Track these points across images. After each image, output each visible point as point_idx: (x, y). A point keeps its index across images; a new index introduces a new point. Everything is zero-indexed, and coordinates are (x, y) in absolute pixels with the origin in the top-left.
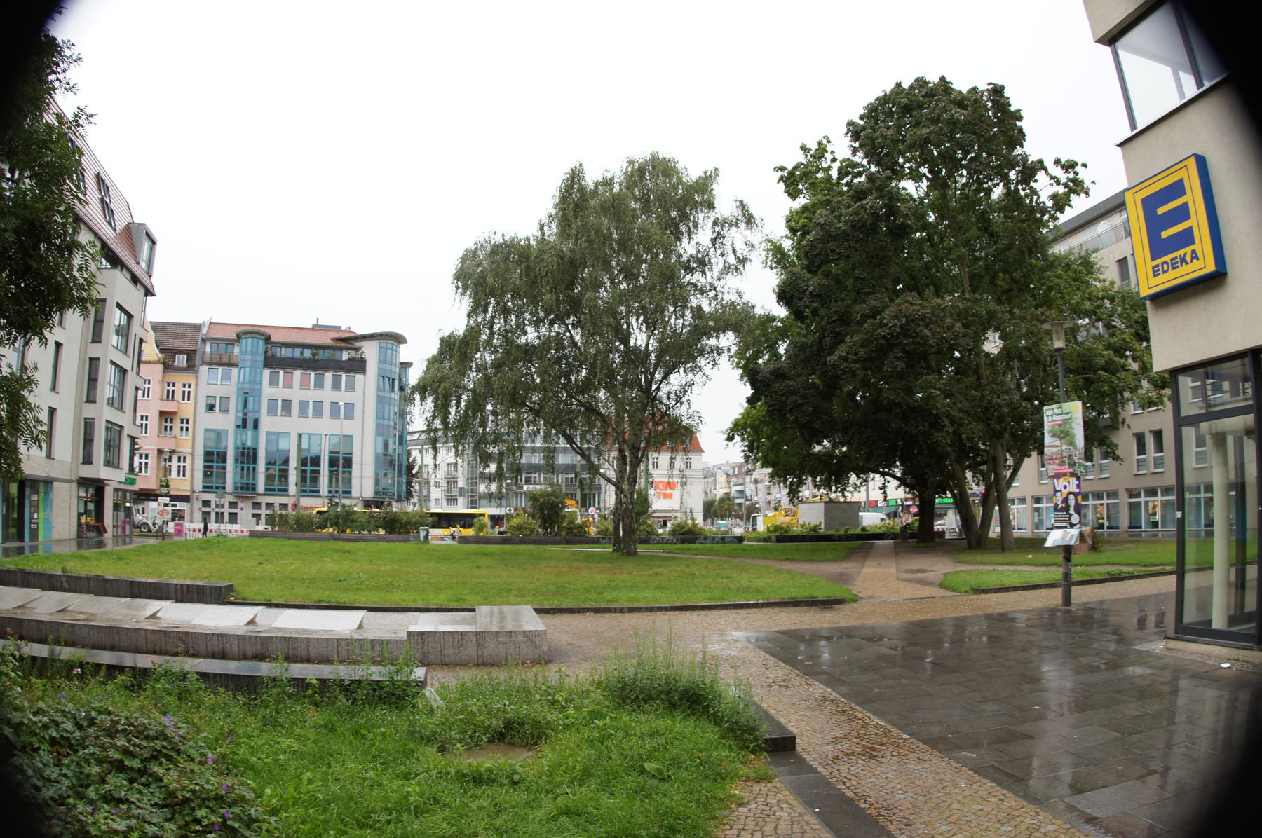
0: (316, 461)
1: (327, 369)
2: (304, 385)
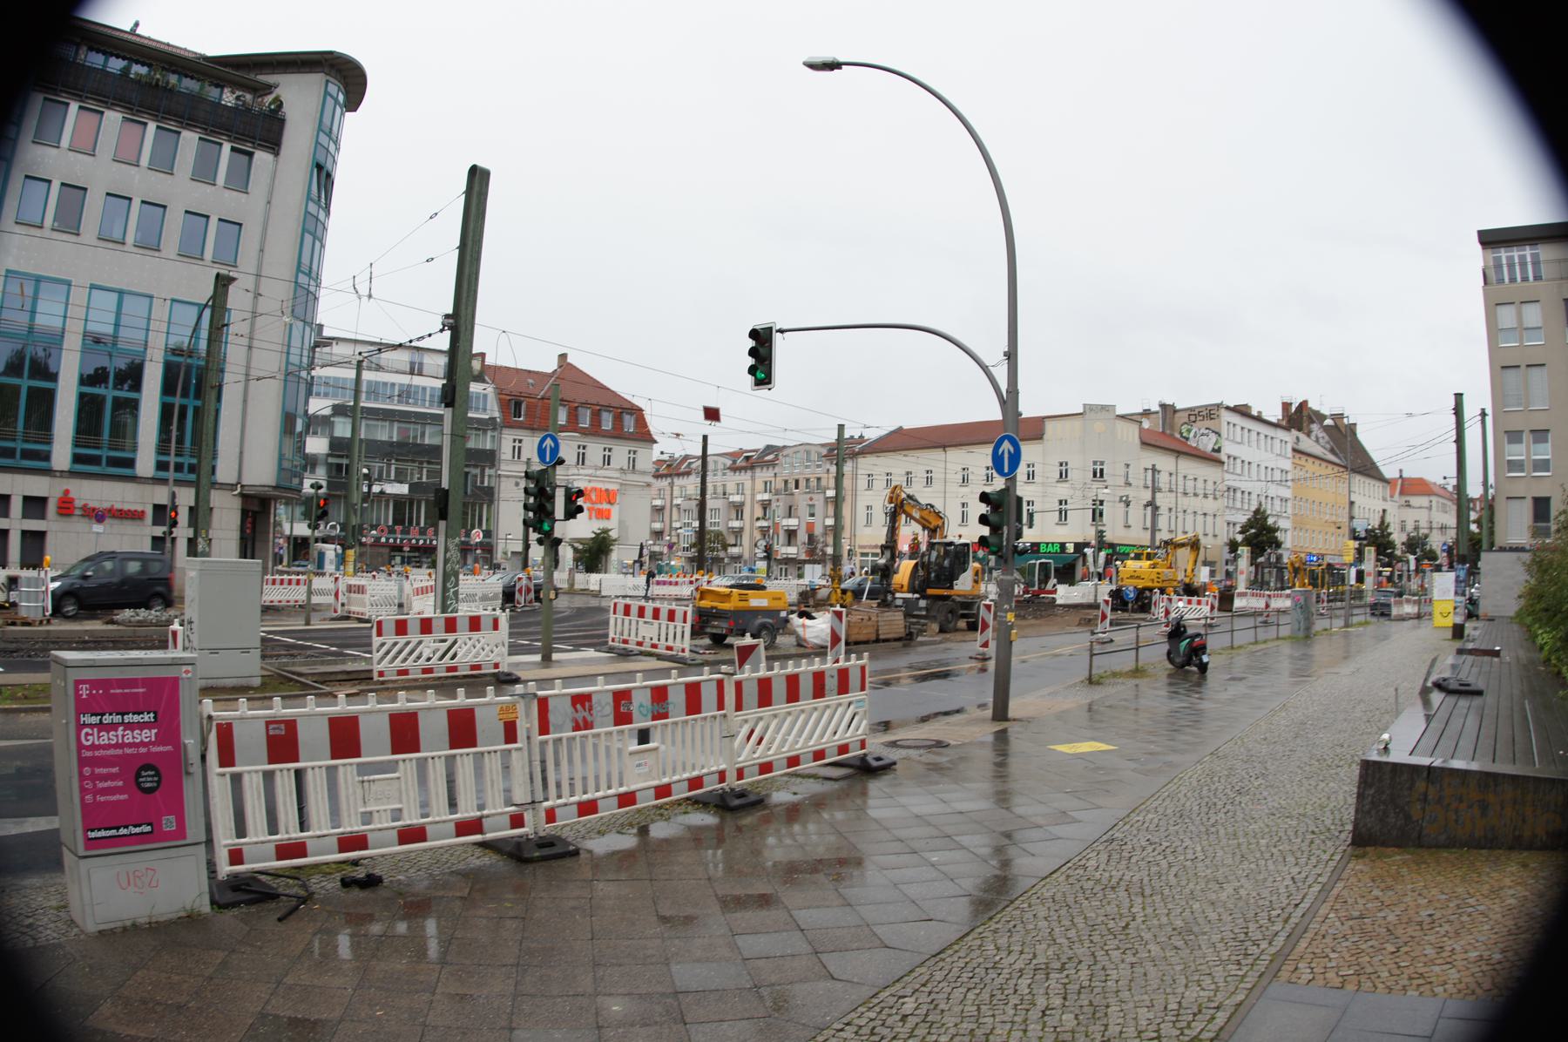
0: (133, 376)
1: (190, 122)
2: (205, 173)
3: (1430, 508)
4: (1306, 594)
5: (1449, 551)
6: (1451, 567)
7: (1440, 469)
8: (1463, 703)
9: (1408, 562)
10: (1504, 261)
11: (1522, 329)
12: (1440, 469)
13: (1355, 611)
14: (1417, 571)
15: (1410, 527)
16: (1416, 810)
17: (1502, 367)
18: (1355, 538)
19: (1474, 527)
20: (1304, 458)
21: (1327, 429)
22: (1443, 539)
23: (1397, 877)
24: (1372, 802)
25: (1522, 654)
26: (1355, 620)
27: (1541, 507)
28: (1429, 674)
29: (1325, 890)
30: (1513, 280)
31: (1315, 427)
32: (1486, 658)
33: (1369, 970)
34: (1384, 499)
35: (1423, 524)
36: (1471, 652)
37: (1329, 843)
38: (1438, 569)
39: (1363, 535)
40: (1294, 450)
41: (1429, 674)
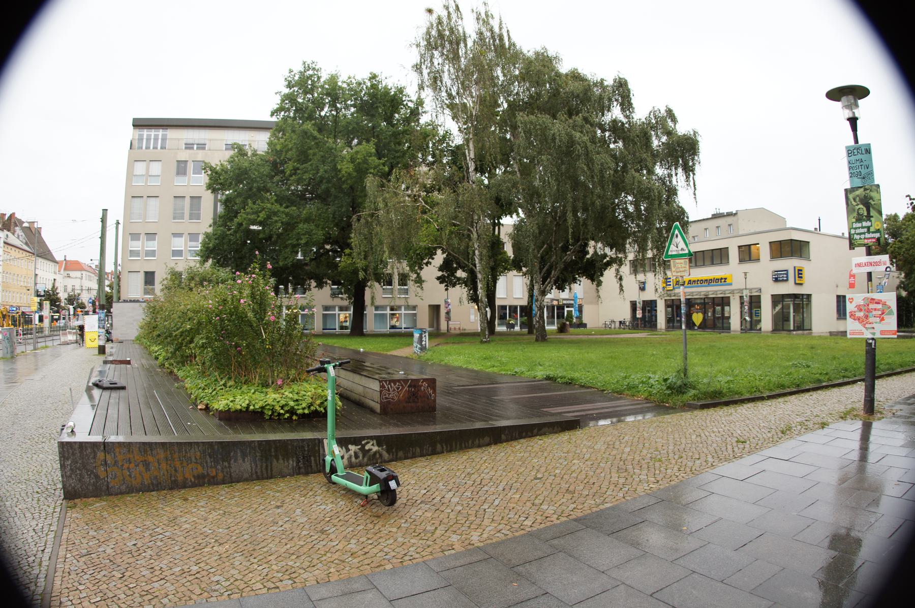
3: (82, 278)
4: (10, 330)
5: (93, 303)
6: (94, 312)
7: (89, 255)
8: (115, 394)
9: (69, 310)
10: (145, 137)
11: (148, 175)
12: (89, 255)
13: (39, 340)
14: (74, 314)
15: (69, 289)
16: (101, 471)
17: (133, 196)
18: (38, 296)
19: (107, 289)
20: (10, 247)
21: (24, 229)
22: (89, 296)
23: (102, 519)
24: (71, 469)
25: (144, 361)
26: (40, 345)
27: (149, 278)
28: (90, 378)
29: (58, 536)
30: (148, 148)
31: (17, 229)
32: (123, 366)
33: (110, 595)
34: (55, 273)
35: (78, 287)
36: (112, 362)
37: (50, 500)
38: (87, 313)
39: (42, 293)
40: (5, 243)
41: (90, 378)
